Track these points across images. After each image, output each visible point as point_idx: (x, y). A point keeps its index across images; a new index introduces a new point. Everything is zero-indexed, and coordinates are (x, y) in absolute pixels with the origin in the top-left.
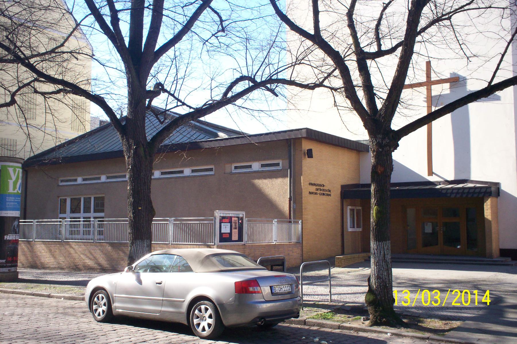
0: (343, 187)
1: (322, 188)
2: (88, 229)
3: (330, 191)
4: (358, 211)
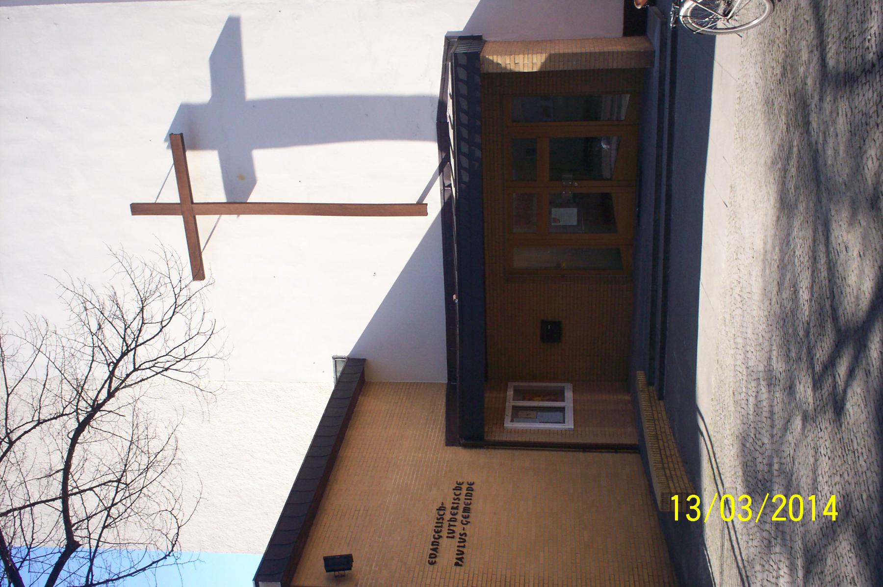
0: (450, 441)
1: (448, 516)
3: (458, 488)
4: (521, 394)
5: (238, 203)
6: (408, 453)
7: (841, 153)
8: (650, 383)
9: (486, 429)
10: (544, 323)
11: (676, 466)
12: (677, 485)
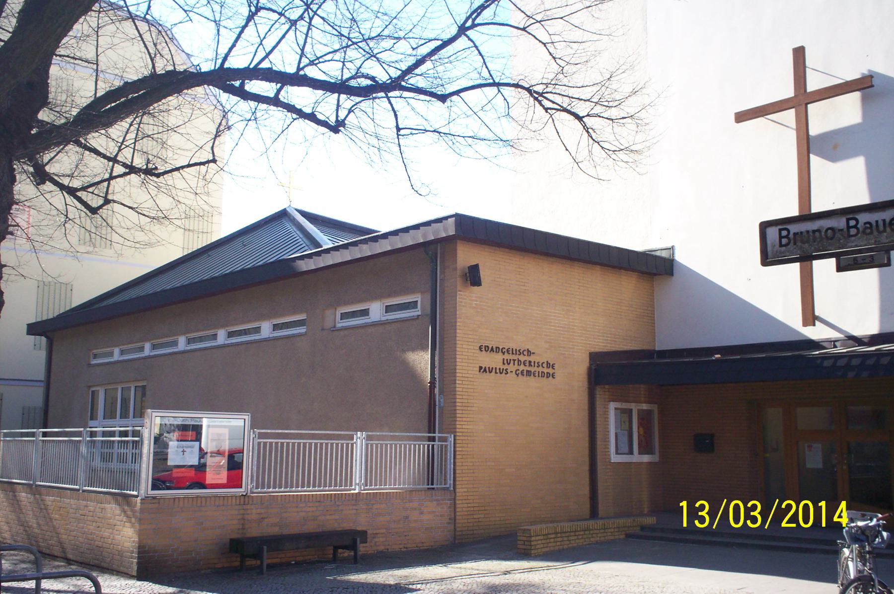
0: (594, 357)
1: (522, 358)
2: (108, 451)
4: (645, 419)
5: (808, 146)
6: (583, 321)
7: (483, 579)
8: (643, 528)
9: (607, 387)
10: (712, 436)
11: (559, 543)
12: (539, 542)
